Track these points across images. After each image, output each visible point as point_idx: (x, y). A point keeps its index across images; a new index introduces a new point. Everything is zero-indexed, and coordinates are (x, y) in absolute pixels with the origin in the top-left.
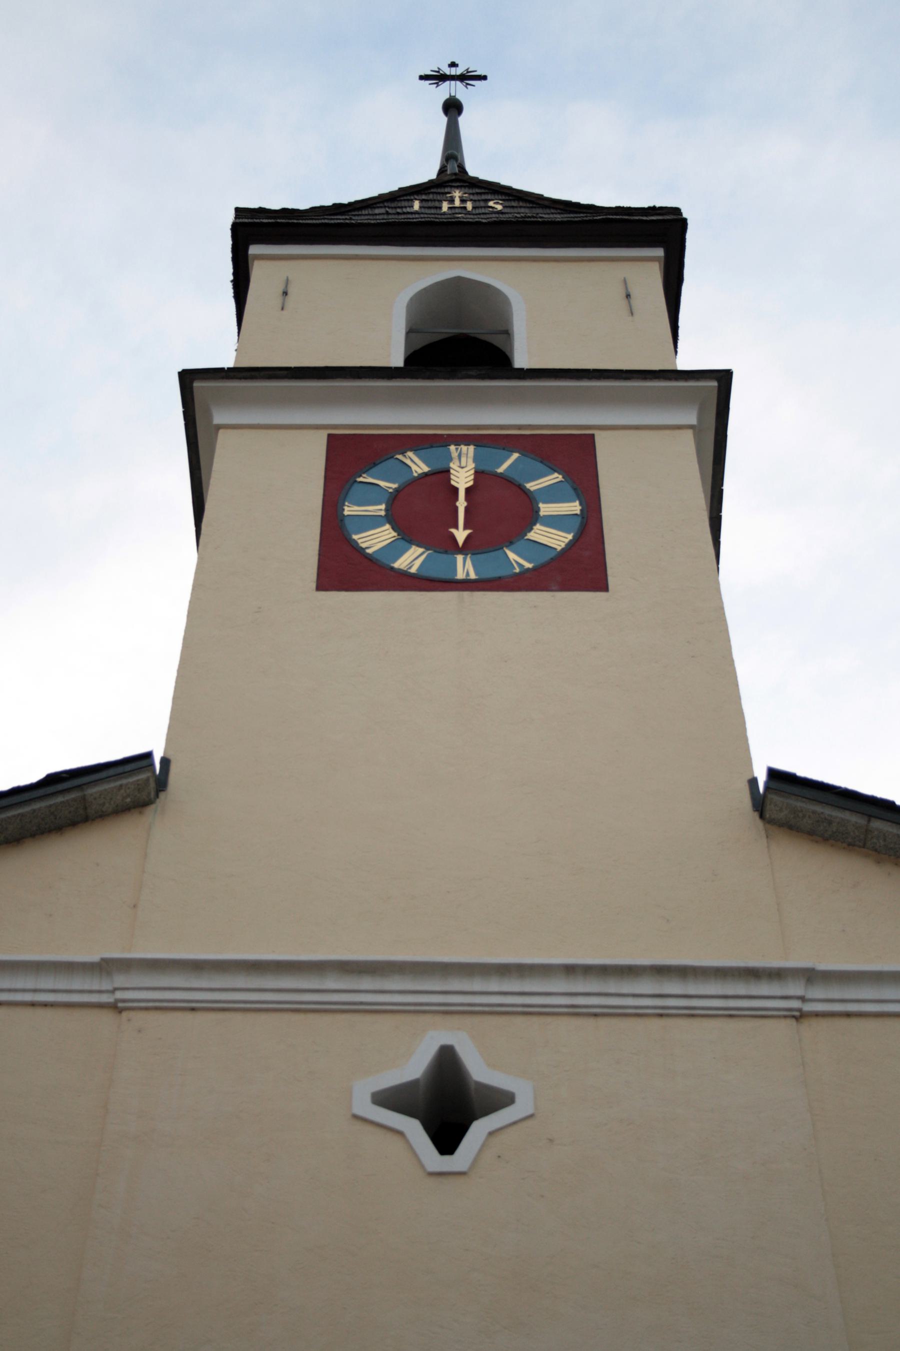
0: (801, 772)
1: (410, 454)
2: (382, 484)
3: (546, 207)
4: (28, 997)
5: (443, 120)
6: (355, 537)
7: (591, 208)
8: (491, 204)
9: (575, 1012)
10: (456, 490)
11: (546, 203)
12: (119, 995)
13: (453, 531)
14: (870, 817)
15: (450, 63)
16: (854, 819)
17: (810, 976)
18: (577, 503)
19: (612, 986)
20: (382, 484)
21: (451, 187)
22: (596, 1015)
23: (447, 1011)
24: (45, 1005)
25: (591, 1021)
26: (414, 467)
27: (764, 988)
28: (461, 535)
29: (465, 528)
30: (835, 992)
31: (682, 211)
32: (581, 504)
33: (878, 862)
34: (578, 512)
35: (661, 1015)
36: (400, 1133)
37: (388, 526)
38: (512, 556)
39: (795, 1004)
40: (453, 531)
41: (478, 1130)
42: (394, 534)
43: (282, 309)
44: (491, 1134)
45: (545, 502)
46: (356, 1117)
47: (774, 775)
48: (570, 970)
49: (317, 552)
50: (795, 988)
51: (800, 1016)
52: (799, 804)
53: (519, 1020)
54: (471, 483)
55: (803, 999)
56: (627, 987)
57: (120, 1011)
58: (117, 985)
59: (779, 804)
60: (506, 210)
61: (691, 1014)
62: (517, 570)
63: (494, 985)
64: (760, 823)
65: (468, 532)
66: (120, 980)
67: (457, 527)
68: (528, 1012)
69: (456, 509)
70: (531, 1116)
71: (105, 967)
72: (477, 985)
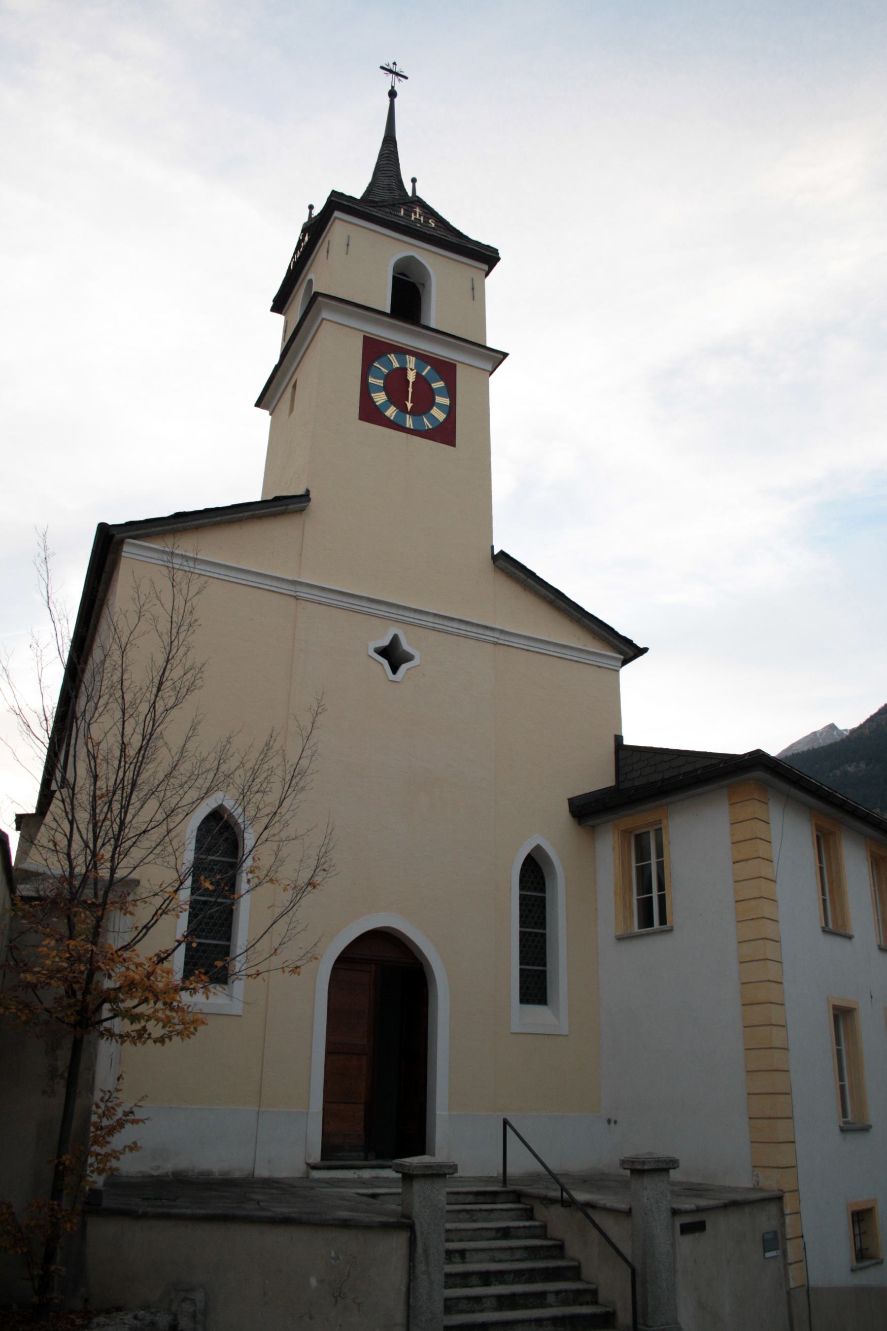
0: (511, 555)
1: (393, 355)
2: (383, 369)
3: (451, 231)
4: (268, 588)
5: (388, 99)
6: (373, 395)
7: (466, 238)
8: (430, 221)
9: (434, 629)
10: (408, 382)
11: (452, 229)
12: (298, 594)
13: (406, 402)
14: (528, 577)
15: (871, 1130)
16: (523, 576)
17: (502, 632)
18: (448, 400)
19: (446, 623)
20: (383, 369)
21: (416, 204)
22: (439, 631)
23: (397, 621)
24: (273, 591)
25: (437, 633)
26: (394, 363)
27: (488, 633)
28: (409, 405)
29: (411, 403)
30: (507, 638)
31: (499, 252)
32: (450, 401)
33: (525, 590)
34: (448, 404)
35: (458, 635)
36: (382, 664)
37: (384, 393)
38: (425, 420)
39: (495, 640)
40: (406, 402)
41: (404, 668)
42: (386, 397)
43: (347, 254)
44: (407, 669)
45: (438, 396)
46: (369, 656)
47: (502, 553)
48: (435, 615)
49: (359, 399)
50: (497, 635)
51: (496, 644)
52: (507, 565)
53: (417, 628)
54: (414, 380)
55: (498, 638)
56: (450, 624)
57: (297, 599)
58: (297, 590)
59: (501, 563)
60: (437, 228)
61: (466, 637)
62: (426, 428)
63: (412, 615)
64: (493, 566)
65: (412, 404)
66: (298, 588)
67: (408, 401)
68: (420, 626)
69: (408, 391)
70: (419, 665)
71: (294, 583)
72: (407, 614)
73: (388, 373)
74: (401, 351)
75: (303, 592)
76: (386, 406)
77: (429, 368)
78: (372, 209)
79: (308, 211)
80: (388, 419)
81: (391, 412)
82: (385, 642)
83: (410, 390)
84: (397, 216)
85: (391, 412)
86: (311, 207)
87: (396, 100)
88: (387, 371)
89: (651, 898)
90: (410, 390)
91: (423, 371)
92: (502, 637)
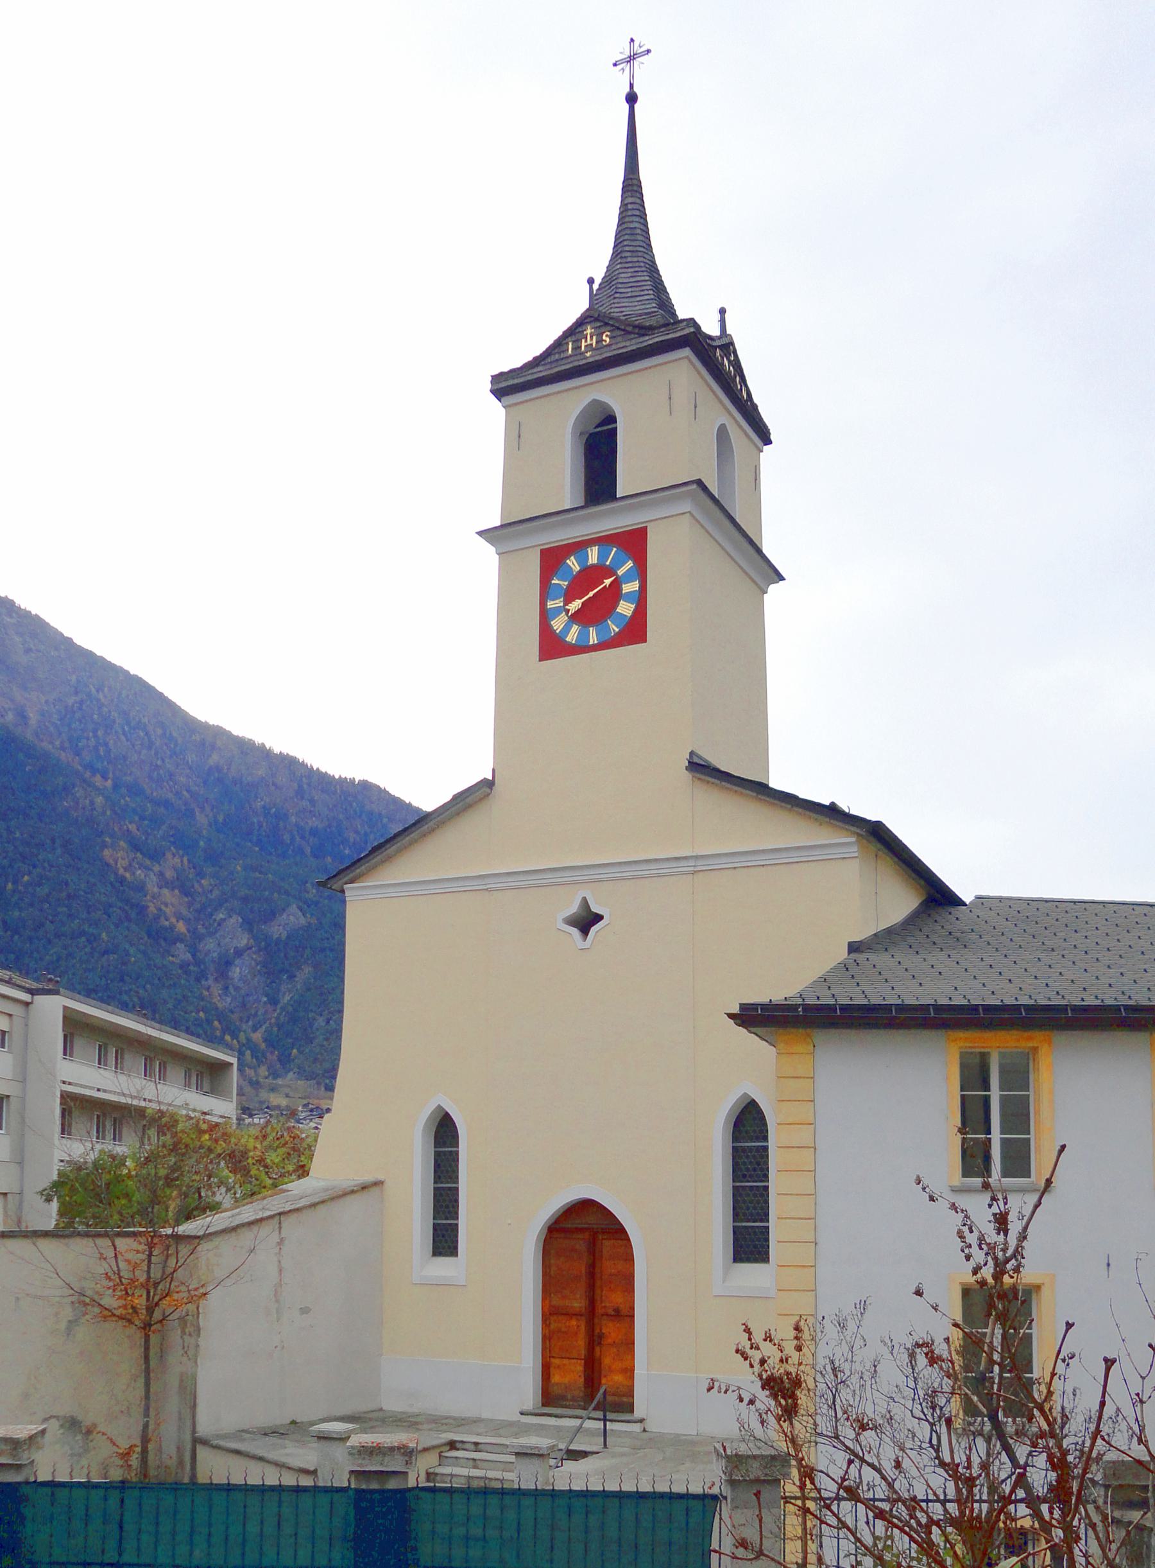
5: (627, 106)
17: (697, 857)
39: (692, 869)
73: (568, 586)
74: (578, 547)
75: (701, 865)
76: (628, 597)
77: (615, 549)
78: (535, 370)
79: (588, 286)
80: (636, 612)
81: (626, 609)
82: (575, 932)
83: (591, 594)
84: (567, 357)
85: (626, 609)
86: (591, 281)
87: (636, 106)
88: (566, 583)
89: (986, 1101)
90: (591, 594)
91: (607, 561)
92: (700, 862)
